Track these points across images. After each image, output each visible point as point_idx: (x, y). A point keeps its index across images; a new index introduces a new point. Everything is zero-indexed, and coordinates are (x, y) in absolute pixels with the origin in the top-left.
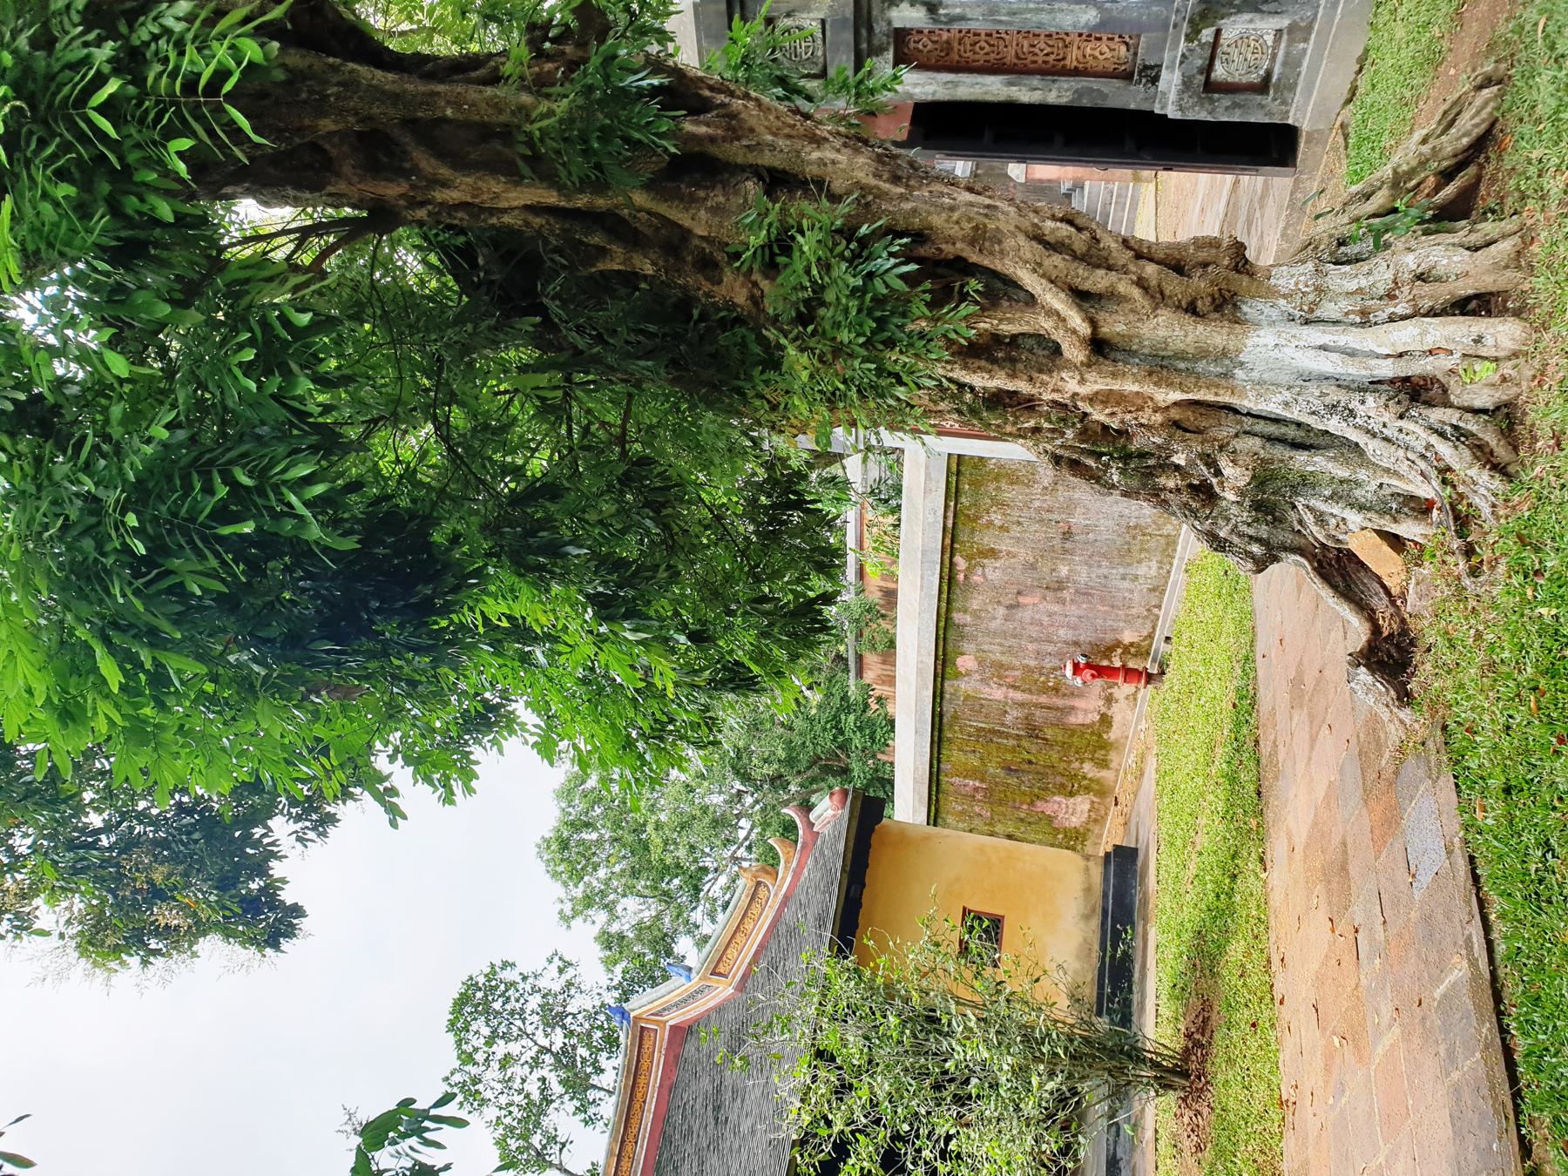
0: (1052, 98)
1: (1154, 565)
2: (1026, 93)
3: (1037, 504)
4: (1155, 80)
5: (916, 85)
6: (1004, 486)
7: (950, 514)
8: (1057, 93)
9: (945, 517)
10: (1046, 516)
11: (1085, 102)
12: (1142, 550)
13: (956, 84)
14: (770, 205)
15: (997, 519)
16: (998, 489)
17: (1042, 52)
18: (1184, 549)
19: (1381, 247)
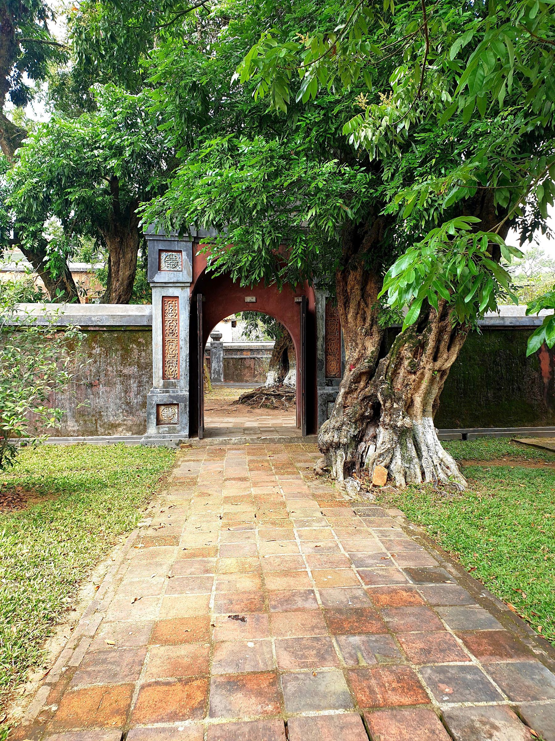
0: (319, 352)
1: (76, 428)
2: (320, 343)
3: (110, 369)
4: (328, 385)
5: (321, 305)
6: (119, 353)
7: (97, 329)
8: (320, 354)
9: (95, 326)
10: (102, 375)
11: (318, 364)
12: (85, 421)
13: (322, 319)
14: (394, 567)
15: (97, 351)
16: (117, 350)
17: (333, 347)
18: (92, 439)
19: (169, 721)
